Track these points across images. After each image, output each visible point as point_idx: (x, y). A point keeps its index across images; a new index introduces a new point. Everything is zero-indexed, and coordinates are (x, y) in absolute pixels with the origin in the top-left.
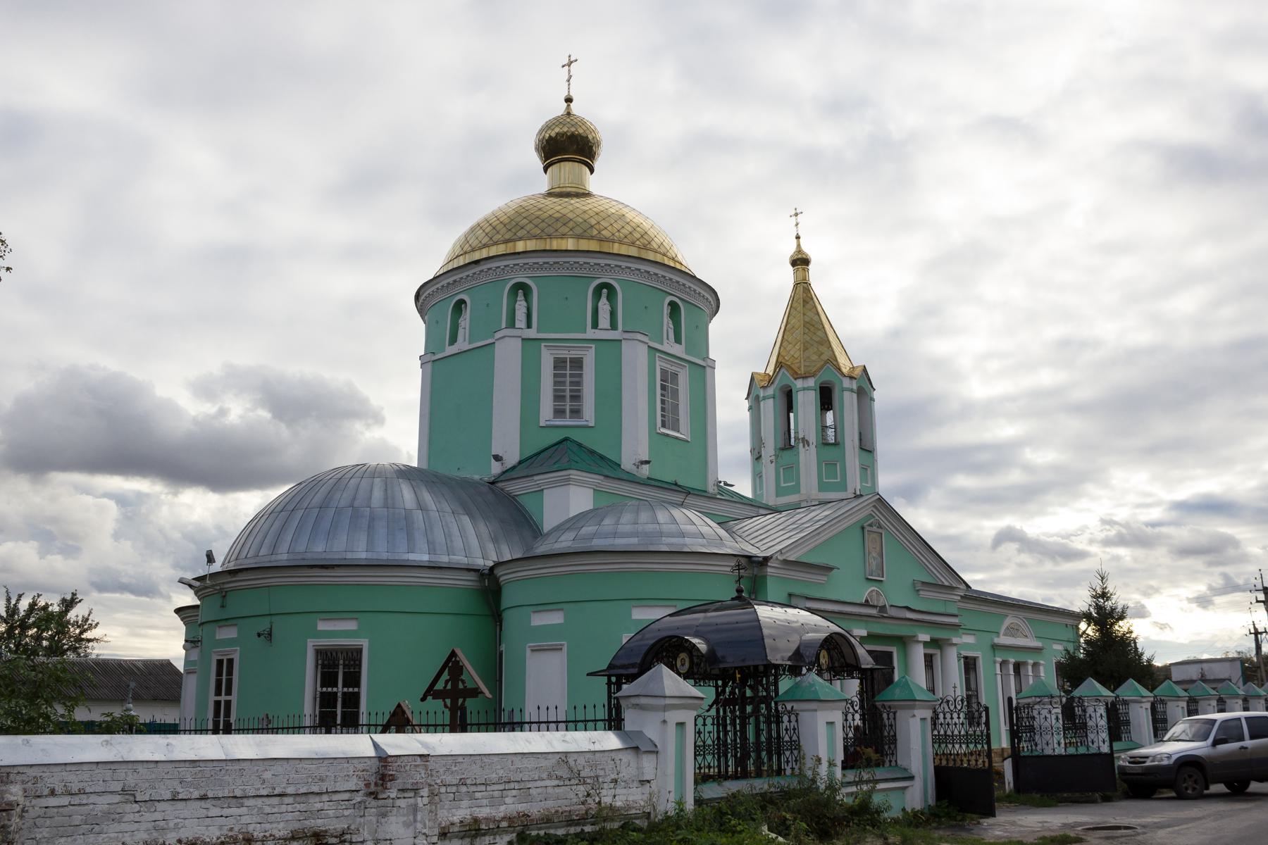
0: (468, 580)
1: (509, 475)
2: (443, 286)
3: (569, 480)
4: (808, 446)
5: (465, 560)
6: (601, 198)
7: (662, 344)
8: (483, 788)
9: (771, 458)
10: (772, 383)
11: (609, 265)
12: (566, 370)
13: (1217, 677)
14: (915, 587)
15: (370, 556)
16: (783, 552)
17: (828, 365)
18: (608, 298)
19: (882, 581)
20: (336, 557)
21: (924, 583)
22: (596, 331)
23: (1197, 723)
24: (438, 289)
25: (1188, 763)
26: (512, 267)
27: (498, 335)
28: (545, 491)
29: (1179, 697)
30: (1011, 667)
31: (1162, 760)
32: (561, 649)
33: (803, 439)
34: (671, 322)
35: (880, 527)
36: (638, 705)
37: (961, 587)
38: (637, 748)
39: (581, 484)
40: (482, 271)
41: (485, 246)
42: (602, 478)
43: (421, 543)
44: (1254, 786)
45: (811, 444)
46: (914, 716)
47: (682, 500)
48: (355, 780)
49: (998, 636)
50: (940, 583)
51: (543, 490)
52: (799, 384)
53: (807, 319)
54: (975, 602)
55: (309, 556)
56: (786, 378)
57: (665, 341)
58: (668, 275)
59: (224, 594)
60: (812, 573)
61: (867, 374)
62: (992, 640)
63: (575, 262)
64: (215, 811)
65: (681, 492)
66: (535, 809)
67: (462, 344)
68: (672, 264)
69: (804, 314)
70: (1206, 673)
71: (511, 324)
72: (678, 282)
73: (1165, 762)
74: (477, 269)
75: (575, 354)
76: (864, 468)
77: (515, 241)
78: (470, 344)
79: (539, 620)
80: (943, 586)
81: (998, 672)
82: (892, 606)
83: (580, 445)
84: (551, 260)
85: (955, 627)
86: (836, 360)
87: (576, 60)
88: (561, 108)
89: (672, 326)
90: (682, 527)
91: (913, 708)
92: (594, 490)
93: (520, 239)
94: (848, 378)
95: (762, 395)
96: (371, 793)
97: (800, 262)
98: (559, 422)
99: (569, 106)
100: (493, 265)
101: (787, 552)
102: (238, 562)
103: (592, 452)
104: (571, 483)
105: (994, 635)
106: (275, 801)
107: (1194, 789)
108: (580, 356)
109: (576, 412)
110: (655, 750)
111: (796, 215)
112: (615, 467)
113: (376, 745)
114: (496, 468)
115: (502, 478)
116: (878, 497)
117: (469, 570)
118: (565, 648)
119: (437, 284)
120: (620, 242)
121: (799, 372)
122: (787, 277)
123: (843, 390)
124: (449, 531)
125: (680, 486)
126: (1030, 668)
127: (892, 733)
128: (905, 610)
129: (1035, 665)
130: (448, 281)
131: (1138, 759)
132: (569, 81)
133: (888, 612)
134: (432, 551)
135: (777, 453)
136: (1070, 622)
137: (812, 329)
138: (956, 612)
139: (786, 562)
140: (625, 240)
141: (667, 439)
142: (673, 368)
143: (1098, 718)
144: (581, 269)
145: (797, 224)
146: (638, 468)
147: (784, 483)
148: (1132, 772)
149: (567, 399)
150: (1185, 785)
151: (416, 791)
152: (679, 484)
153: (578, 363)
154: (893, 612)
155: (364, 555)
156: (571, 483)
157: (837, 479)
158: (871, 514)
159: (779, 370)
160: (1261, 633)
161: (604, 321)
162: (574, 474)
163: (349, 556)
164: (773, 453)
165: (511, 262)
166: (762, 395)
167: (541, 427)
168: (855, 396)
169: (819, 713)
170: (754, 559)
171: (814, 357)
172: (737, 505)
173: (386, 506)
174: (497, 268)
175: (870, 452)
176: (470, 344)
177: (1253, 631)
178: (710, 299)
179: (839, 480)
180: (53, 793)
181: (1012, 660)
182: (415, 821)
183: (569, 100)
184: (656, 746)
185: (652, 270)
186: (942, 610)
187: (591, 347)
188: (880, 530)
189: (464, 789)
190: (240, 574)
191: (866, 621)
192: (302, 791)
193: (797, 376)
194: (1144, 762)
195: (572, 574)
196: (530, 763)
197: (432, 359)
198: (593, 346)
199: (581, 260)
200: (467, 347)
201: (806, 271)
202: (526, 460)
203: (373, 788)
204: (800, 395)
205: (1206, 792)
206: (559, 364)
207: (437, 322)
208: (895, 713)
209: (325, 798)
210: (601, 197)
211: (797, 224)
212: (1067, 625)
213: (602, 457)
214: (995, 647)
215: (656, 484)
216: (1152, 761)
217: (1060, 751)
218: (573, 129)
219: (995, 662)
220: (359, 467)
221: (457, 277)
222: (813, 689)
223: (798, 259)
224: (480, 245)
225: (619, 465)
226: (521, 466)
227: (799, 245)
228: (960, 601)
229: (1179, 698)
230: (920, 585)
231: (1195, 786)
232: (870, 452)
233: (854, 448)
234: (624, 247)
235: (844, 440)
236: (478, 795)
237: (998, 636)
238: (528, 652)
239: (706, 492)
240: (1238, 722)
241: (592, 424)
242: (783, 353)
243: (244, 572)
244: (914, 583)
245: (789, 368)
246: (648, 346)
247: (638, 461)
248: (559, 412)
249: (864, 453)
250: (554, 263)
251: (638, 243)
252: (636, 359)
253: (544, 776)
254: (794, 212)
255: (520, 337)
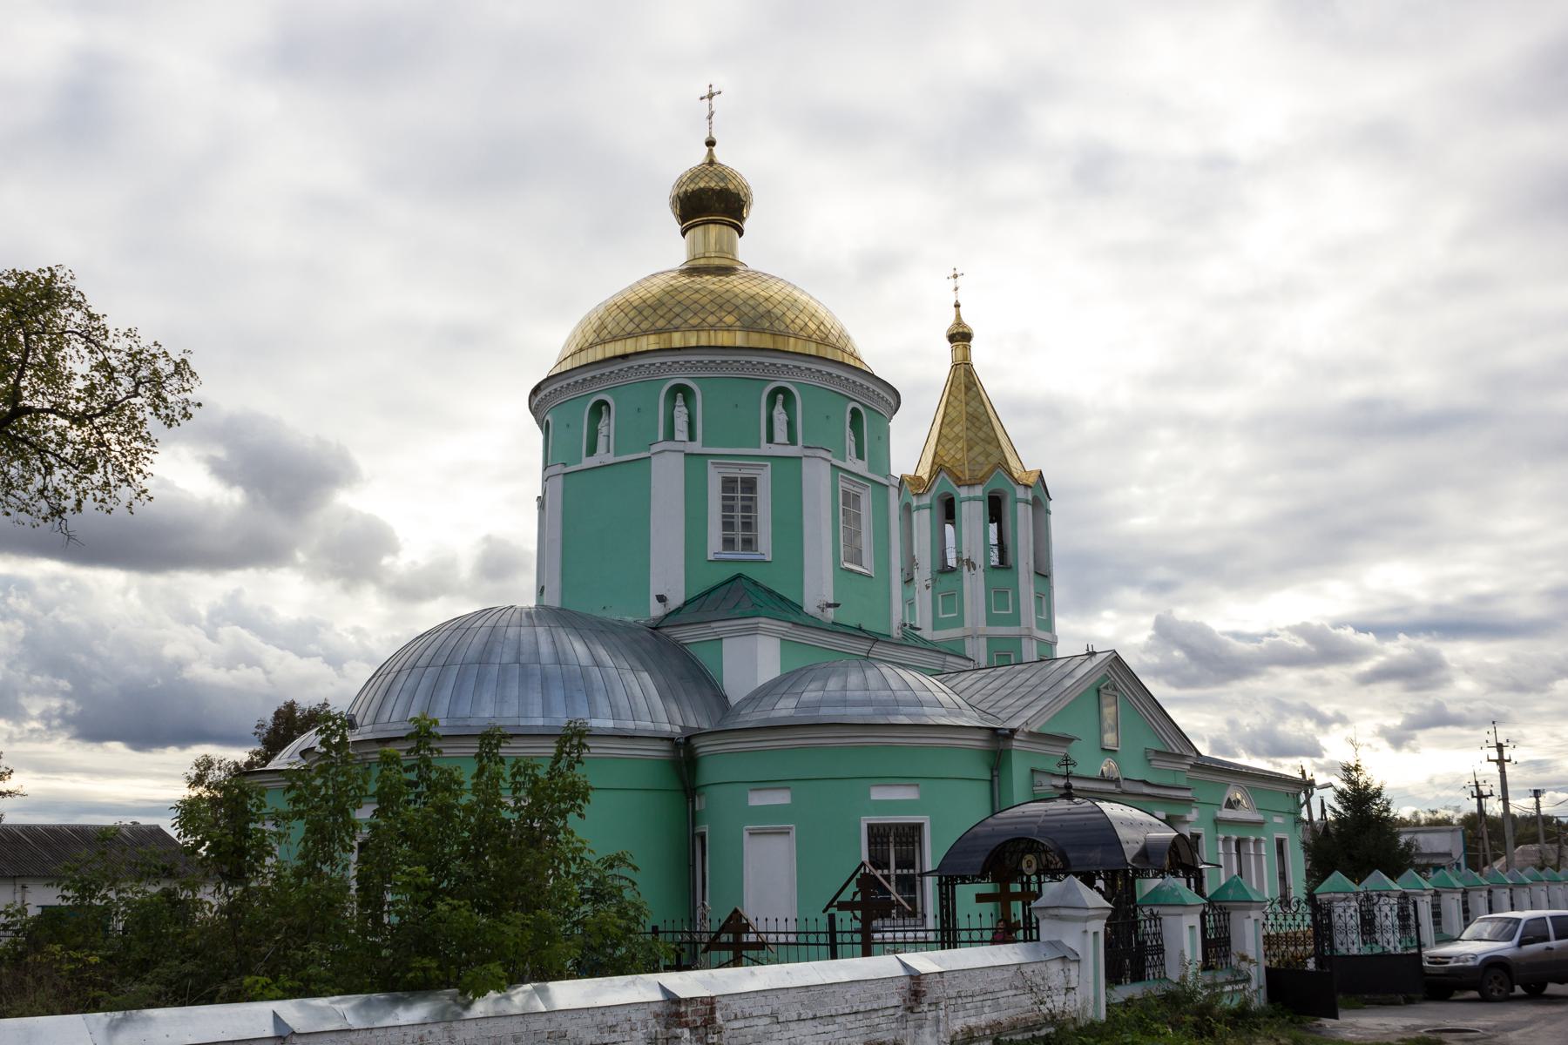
0: (659, 751)
1: (675, 617)
2: (576, 382)
3: (757, 629)
4: (975, 569)
5: (651, 726)
6: (765, 277)
7: (845, 461)
8: (970, 999)
9: (927, 583)
10: (929, 490)
11: (787, 366)
12: (741, 493)
13: (1435, 851)
14: (1146, 756)
15: (547, 722)
16: (1029, 722)
17: (999, 470)
18: (785, 406)
19: (1115, 751)
20: (508, 723)
21: (1157, 752)
22: (770, 445)
23: (1500, 921)
24: (569, 385)
25: (1494, 964)
26: (670, 366)
27: (655, 448)
28: (724, 640)
29: (1456, 888)
30: (1233, 844)
31: (1467, 961)
32: (789, 833)
33: (968, 560)
34: (852, 433)
35: (1115, 689)
36: (1057, 916)
37: (1192, 755)
38: (1065, 957)
39: (769, 633)
40: (632, 367)
41: (630, 335)
42: (790, 625)
43: (602, 702)
44: (1552, 988)
45: (977, 566)
46: (1249, 917)
47: (873, 649)
48: (897, 997)
49: (1220, 810)
50: (1170, 751)
51: (721, 639)
52: (963, 492)
53: (970, 410)
54: (1199, 771)
55: (473, 722)
56: (945, 484)
57: (848, 457)
58: (852, 377)
59: (367, 765)
60: (1039, 743)
61: (1043, 481)
62: (1215, 813)
63: (747, 362)
64: (821, 1029)
65: (867, 638)
66: (1004, 1017)
67: (602, 456)
68: (852, 362)
69: (967, 404)
70: (1421, 846)
71: (670, 435)
72: (861, 385)
73: (1471, 963)
74: (625, 365)
75: (747, 473)
76: (1039, 598)
77: (669, 331)
78: (615, 455)
79: (757, 799)
80: (1173, 755)
81: (1221, 851)
82: (1125, 779)
83: (755, 583)
84: (719, 359)
85: (1188, 802)
86: (1008, 464)
87: (720, 93)
88: (699, 156)
89: (853, 438)
90: (918, 693)
91: (1249, 909)
92: (781, 639)
93: (677, 329)
94: (1023, 487)
95: (915, 504)
96: (909, 1008)
97: (960, 336)
98: (728, 555)
99: (711, 151)
100: (646, 361)
101: (1032, 722)
102: (378, 727)
103: (770, 592)
104: (759, 632)
105: (1215, 808)
106: (852, 1018)
107: (1499, 991)
108: (755, 476)
109: (749, 543)
110: (1077, 958)
111: (955, 276)
112: (797, 609)
113: (905, 965)
114: (656, 610)
115: (666, 622)
116: (1115, 655)
117: (662, 739)
118: (793, 833)
119: (568, 378)
120: (797, 337)
121: (963, 478)
122: (944, 353)
123: (1017, 501)
124: (632, 693)
125: (864, 631)
126: (1251, 845)
127: (1227, 935)
128: (1141, 784)
129: (1257, 842)
130: (584, 376)
131: (1440, 959)
132: (710, 118)
133: (1122, 786)
134: (615, 716)
135: (935, 576)
136: (1291, 790)
137: (977, 424)
138: (1183, 783)
139: (1031, 734)
140: (802, 333)
141: (851, 576)
142: (855, 489)
143: (1387, 913)
144: (753, 369)
145: (956, 289)
146: (823, 611)
147: (943, 614)
148: (1433, 972)
149: (740, 528)
150: (1490, 987)
151: (936, 1004)
152: (864, 628)
153: (750, 485)
154: (1127, 786)
155: (540, 722)
156: (759, 632)
157: (1008, 610)
158: (1106, 675)
159: (936, 478)
160: (1486, 797)
161: (781, 434)
162: (763, 622)
163: (523, 722)
164: (929, 576)
165: (669, 359)
166: (915, 504)
167: (710, 561)
168: (1030, 508)
169: (1184, 917)
170: (1000, 731)
171: (981, 459)
172: (925, 652)
173: (558, 662)
174: (651, 365)
175: (1046, 576)
176: (615, 455)
177: (1475, 794)
178: (890, 400)
179: (1010, 612)
180: (736, 1018)
181: (1235, 837)
182: (938, 1031)
183: (711, 143)
184: (1077, 955)
185: (835, 371)
186: (1169, 781)
187: (766, 466)
188: (1115, 693)
189: (960, 1001)
190: (391, 744)
191: (650, 699)
192: (869, 1008)
193: (959, 482)
194: (1447, 963)
195: (801, 747)
196: (998, 975)
197: (563, 472)
198: (769, 464)
199: (755, 359)
200: (611, 459)
201: (967, 349)
202: (694, 600)
203: (909, 1004)
204: (965, 506)
205: (1511, 994)
206: (728, 484)
207: (568, 426)
208: (1229, 914)
209: (880, 1014)
210: (765, 274)
211: (956, 289)
212: (1287, 793)
213: (782, 599)
214: (1218, 822)
215: (842, 629)
216: (1456, 962)
217: (1354, 951)
218: (722, 185)
219: (1217, 839)
220: (504, 610)
221: (597, 373)
222: (1177, 893)
223: (958, 333)
224: (623, 333)
225: (801, 608)
226: (687, 608)
227: (958, 316)
228: (1189, 771)
229: (1455, 889)
230: (1153, 753)
231: (1501, 988)
232: (1046, 576)
233: (1028, 573)
234: (800, 342)
235: (1017, 561)
236: (968, 1006)
237: (1220, 810)
238: (746, 834)
239: (889, 636)
240: (1543, 921)
241: (769, 558)
242: (942, 453)
243: (399, 741)
244: (1146, 751)
245: (950, 472)
246: (832, 465)
247: (822, 603)
248: (728, 543)
249: (1040, 579)
250: (723, 362)
251: (814, 336)
252: (817, 479)
253: (1007, 987)
254: (952, 273)
255: (683, 451)
